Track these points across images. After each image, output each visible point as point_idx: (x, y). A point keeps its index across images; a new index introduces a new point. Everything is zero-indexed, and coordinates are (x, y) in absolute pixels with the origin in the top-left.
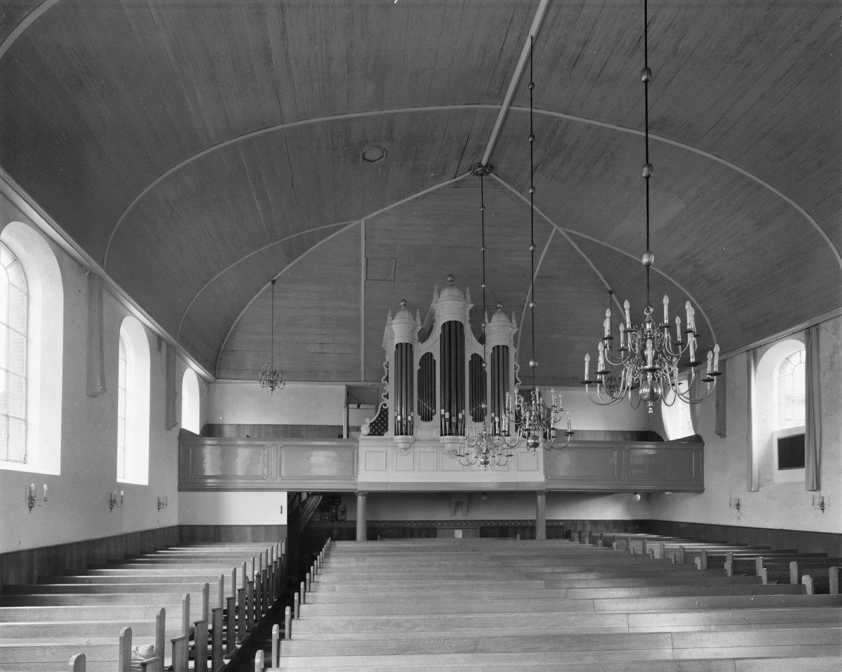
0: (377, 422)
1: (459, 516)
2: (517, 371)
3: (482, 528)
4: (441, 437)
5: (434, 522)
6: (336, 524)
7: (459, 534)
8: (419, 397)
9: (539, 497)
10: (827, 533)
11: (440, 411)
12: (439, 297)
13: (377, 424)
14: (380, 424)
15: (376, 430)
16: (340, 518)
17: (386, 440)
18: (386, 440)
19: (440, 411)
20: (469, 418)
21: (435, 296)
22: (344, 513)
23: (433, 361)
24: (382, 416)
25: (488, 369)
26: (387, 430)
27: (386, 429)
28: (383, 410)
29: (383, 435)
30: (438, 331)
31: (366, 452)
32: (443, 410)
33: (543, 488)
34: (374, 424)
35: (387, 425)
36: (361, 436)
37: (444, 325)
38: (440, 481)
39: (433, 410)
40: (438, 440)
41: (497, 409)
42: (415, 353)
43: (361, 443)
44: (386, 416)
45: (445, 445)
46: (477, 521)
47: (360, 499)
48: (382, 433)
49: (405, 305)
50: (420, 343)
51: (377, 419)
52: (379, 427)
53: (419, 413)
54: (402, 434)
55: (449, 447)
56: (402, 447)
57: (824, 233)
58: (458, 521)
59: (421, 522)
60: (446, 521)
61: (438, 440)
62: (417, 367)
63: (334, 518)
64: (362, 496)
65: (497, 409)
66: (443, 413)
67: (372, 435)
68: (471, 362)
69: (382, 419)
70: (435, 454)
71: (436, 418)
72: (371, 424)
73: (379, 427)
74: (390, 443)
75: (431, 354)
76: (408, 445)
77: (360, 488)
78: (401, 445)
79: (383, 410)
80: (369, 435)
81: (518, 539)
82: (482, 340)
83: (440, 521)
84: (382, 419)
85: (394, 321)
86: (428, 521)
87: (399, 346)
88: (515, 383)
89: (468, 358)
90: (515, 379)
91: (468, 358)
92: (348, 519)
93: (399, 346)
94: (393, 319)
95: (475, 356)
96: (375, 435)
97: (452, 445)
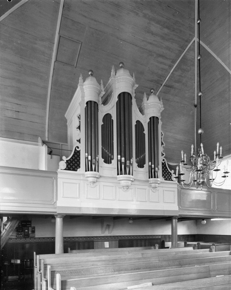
0: (72, 160)
1: (107, 233)
2: (163, 137)
3: (120, 241)
4: (118, 176)
5: (92, 237)
6: (28, 240)
7: (107, 244)
8: (102, 145)
9: (174, 220)
10: (209, 235)
11: (116, 156)
12: (116, 75)
13: (69, 162)
14: (74, 162)
15: (71, 167)
16: (31, 235)
17: (79, 175)
18: (79, 175)
19: (116, 156)
20: (135, 165)
21: (113, 73)
22: (33, 232)
23: (111, 120)
24: (76, 156)
25: (146, 132)
26: (80, 167)
27: (79, 166)
28: (76, 152)
29: (76, 171)
30: (115, 99)
31: (64, 183)
32: (119, 156)
33: (177, 214)
34: (69, 162)
35: (80, 164)
36: (59, 170)
37: (120, 95)
38: (161, 209)
39: (112, 156)
40: (148, 181)
41: (153, 160)
42: (99, 113)
43: (59, 176)
44: (79, 156)
45: (121, 182)
46: (117, 236)
47: (59, 221)
48: (76, 169)
49: (92, 75)
50: (103, 105)
51: (72, 158)
52: (74, 165)
53: (103, 157)
54: (92, 170)
55: (123, 183)
56: (92, 181)
57: (195, 90)
58: (107, 237)
59: (85, 237)
60: (100, 237)
61: (148, 181)
62: (101, 123)
63: (27, 236)
64: (60, 217)
65: (153, 160)
66: (119, 158)
67: (68, 170)
68: (136, 126)
69: (76, 158)
70: (114, 187)
71: (114, 162)
72: (67, 161)
73: (74, 165)
74: (82, 178)
75: (110, 115)
76: (95, 179)
77: (59, 212)
78: (91, 179)
79: (76, 152)
80: (65, 169)
81: (157, 248)
82: (142, 111)
83: (96, 237)
84: (76, 158)
85: (85, 83)
86: (89, 237)
87: (89, 103)
88: (162, 145)
89: (134, 123)
90: (162, 142)
91: (134, 123)
92: (36, 236)
93: (89, 103)
94: (84, 81)
95: (138, 122)
96: (70, 170)
97: (126, 181)
